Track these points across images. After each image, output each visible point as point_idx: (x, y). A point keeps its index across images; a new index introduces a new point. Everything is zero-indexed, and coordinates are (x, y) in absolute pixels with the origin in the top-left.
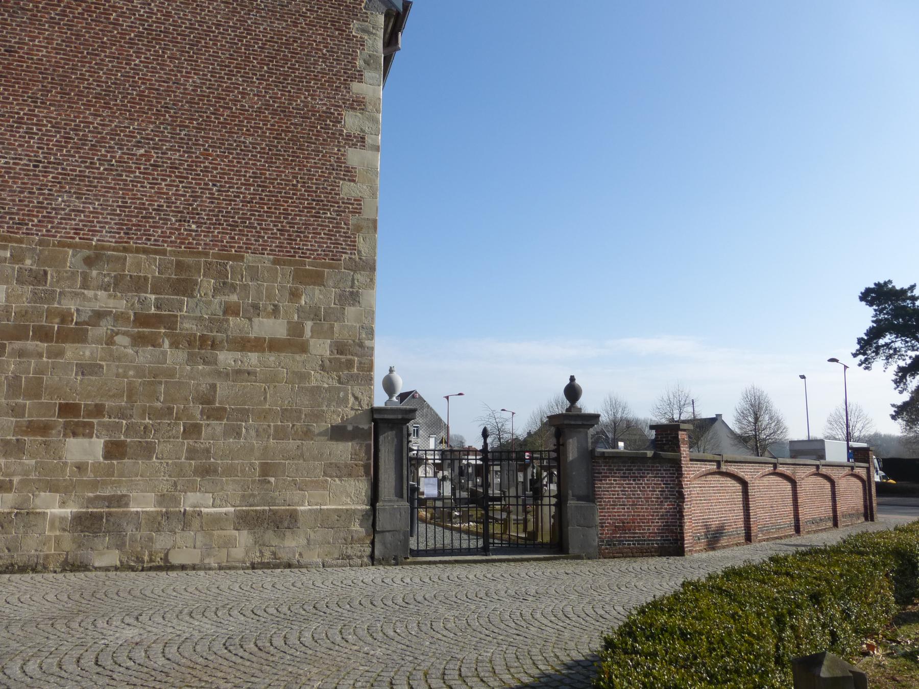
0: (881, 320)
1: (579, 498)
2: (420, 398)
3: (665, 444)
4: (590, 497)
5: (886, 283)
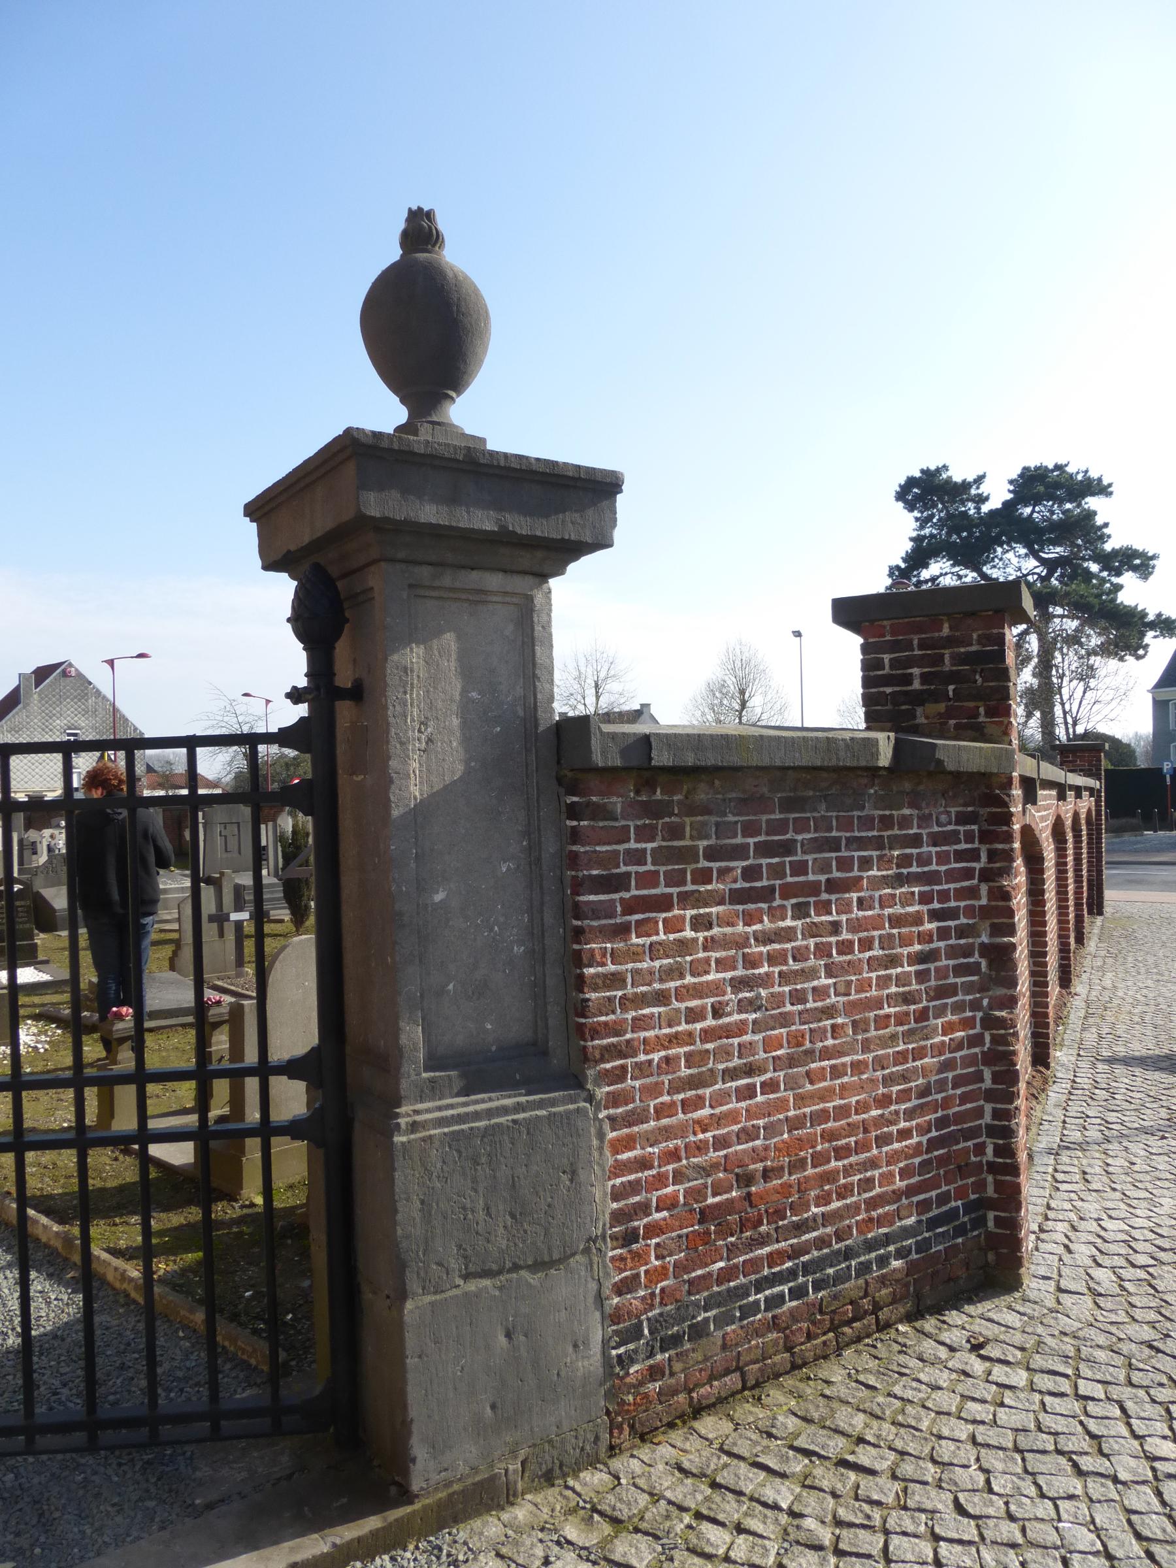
0: (925, 537)
1: (478, 1071)
2: (80, 676)
3: (919, 699)
4: (553, 1051)
5: (938, 470)
